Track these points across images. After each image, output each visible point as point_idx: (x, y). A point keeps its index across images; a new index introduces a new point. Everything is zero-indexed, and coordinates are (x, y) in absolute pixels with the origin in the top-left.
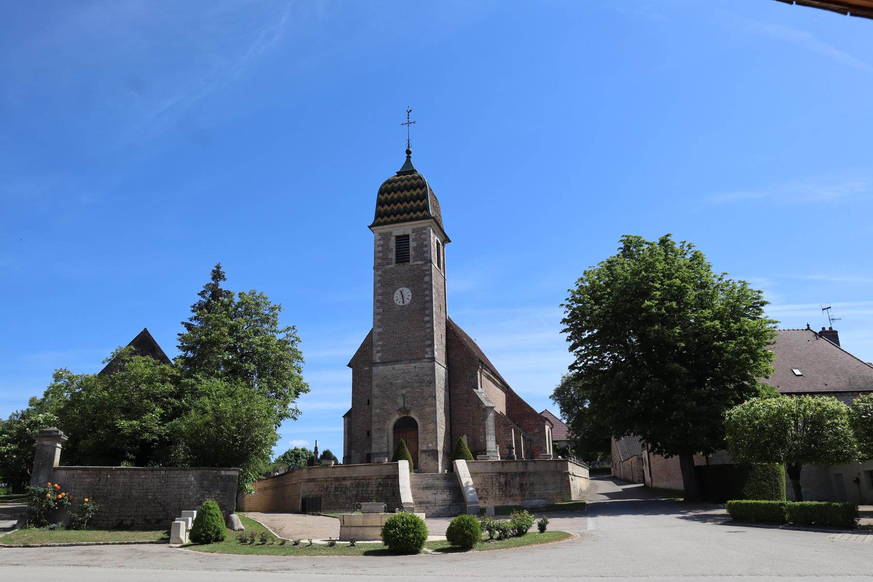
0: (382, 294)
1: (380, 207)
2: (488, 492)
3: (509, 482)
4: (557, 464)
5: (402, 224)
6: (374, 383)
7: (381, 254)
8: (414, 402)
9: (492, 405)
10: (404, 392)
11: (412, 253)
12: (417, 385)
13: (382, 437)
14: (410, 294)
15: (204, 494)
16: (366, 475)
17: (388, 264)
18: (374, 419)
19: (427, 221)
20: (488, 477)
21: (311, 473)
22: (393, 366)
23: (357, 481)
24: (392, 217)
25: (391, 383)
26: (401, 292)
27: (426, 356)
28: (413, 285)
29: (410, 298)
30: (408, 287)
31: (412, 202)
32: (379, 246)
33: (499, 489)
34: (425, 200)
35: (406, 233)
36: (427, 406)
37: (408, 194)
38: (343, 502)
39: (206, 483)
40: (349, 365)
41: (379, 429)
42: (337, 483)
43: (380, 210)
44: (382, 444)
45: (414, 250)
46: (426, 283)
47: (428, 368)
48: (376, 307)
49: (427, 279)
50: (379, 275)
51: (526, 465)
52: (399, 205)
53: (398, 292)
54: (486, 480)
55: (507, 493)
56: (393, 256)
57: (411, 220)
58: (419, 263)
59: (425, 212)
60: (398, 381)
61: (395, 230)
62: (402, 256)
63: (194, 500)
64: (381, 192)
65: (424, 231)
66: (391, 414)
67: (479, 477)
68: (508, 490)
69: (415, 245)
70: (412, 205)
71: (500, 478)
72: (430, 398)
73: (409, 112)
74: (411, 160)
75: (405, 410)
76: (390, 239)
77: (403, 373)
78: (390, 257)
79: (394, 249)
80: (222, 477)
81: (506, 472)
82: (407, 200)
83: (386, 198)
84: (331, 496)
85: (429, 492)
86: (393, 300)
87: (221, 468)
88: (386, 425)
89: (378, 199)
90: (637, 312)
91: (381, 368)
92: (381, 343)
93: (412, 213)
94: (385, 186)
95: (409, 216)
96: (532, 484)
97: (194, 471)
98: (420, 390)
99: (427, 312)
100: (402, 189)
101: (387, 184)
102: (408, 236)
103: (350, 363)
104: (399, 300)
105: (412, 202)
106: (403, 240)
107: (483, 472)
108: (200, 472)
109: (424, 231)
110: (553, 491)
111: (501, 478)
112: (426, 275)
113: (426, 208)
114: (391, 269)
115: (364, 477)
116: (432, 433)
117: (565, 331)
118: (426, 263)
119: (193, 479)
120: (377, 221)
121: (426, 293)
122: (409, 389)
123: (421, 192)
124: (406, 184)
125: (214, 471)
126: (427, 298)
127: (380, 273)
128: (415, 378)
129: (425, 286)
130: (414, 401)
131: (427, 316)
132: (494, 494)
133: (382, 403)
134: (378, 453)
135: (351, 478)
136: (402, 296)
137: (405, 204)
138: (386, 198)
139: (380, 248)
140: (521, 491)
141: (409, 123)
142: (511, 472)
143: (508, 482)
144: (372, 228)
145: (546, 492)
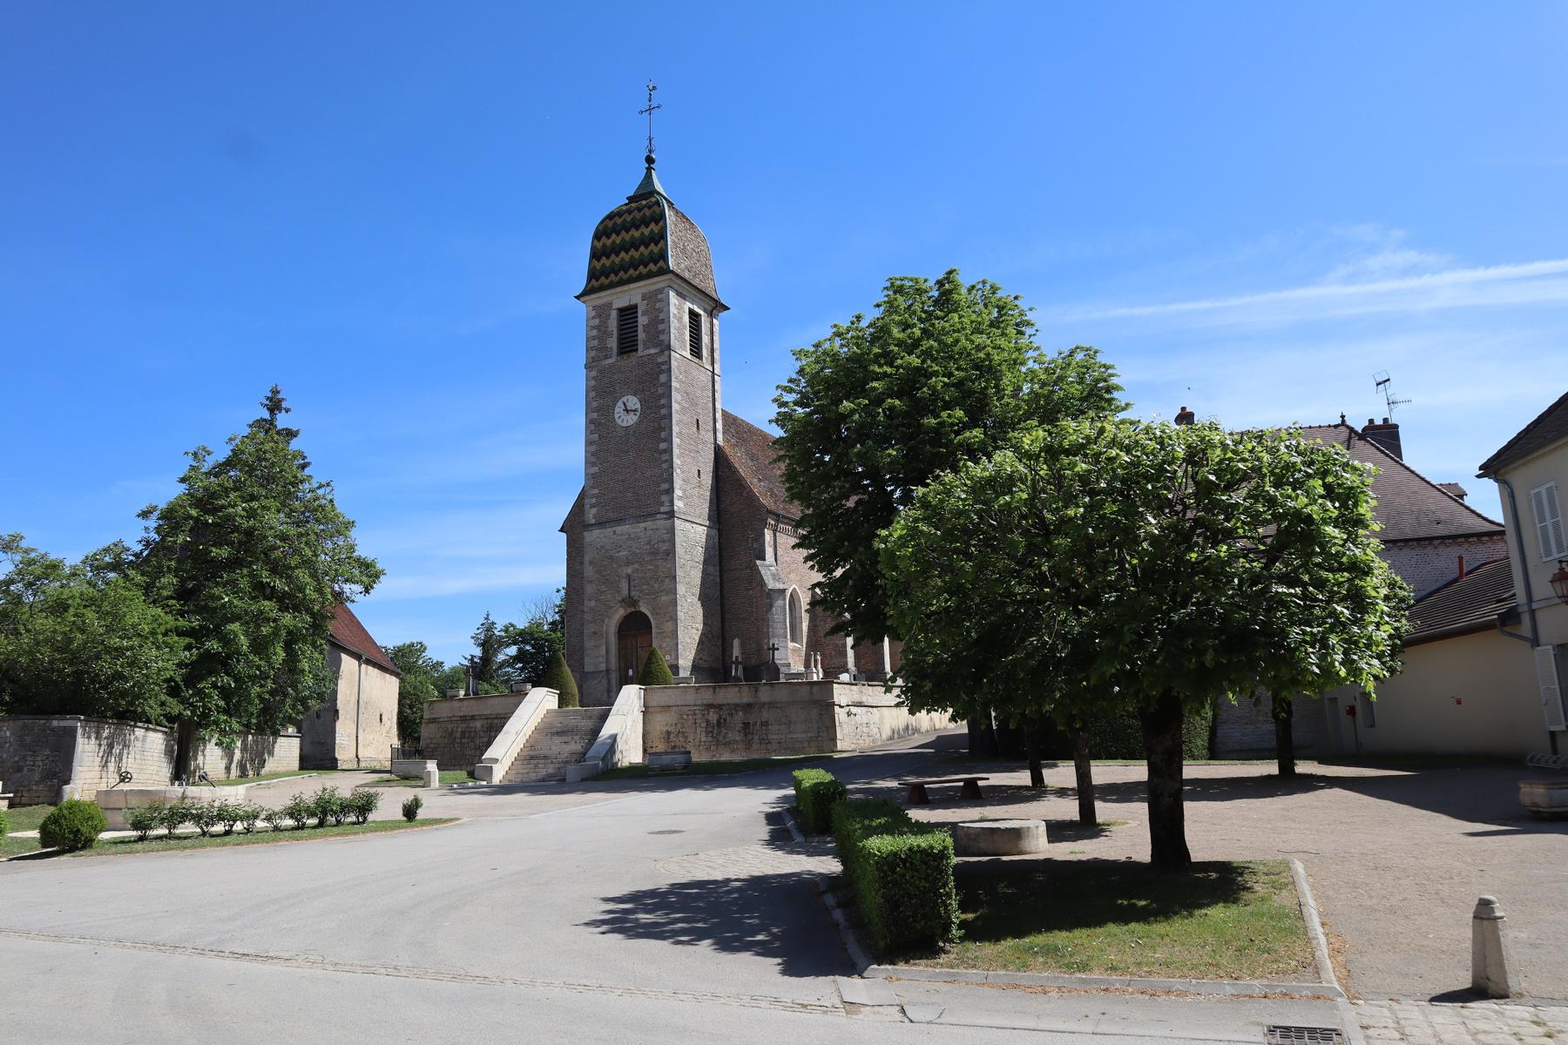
0: (597, 410)
1: (595, 262)
2: (687, 737)
3: (725, 720)
4: (811, 688)
5: (625, 288)
6: (587, 558)
8: (645, 587)
9: (781, 586)
10: (629, 571)
11: (641, 335)
12: (648, 558)
13: (597, 647)
15: (24, 756)
16: (500, 712)
17: (606, 357)
18: (588, 617)
19: (662, 278)
20: (690, 713)
21: (433, 709)
22: (614, 529)
23: (489, 721)
24: (612, 277)
25: (611, 558)
26: (624, 404)
27: (662, 509)
32: (593, 328)
33: (707, 733)
34: (662, 241)
36: (664, 593)
37: (636, 234)
38: (471, 755)
39: (28, 739)
40: (561, 530)
41: (595, 633)
42: (465, 725)
44: (597, 657)
47: (665, 529)
48: (588, 432)
49: (663, 378)
50: (594, 378)
51: (756, 691)
52: (623, 254)
54: (685, 717)
55: (721, 739)
56: (613, 343)
57: (640, 278)
58: (653, 351)
60: (621, 554)
62: (627, 344)
63: (9, 765)
64: (597, 236)
65: (660, 296)
66: (611, 607)
67: (673, 713)
68: (723, 734)
70: (642, 254)
71: (708, 714)
72: (667, 580)
75: (631, 601)
77: (627, 539)
78: (609, 346)
79: (615, 332)
80: (53, 730)
81: (721, 703)
82: (635, 245)
83: (604, 245)
84: (456, 745)
85: (557, 740)
87: (52, 717)
88: (605, 627)
89: (593, 248)
91: (596, 532)
92: (596, 491)
94: (602, 225)
95: (638, 272)
96: (765, 724)
97: (10, 722)
98: (652, 567)
99: (663, 435)
100: (628, 226)
102: (635, 307)
103: (562, 527)
105: (642, 248)
106: (628, 314)
107: (678, 703)
108: (20, 723)
109: (660, 296)
110: (804, 735)
111: (711, 713)
112: (662, 372)
113: (663, 256)
114: (612, 366)
115: (497, 714)
116: (669, 637)
117: (779, 459)
118: (662, 352)
119: (8, 734)
120: (590, 286)
122: (636, 566)
125: (42, 722)
126: (663, 411)
127: (594, 373)
128: (645, 547)
129: (660, 391)
130: (644, 584)
132: (698, 740)
133: (599, 590)
134: (594, 672)
135: (482, 717)
137: (632, 252)
138: (604, 245)
139: (595, 332)
140: (746, 736)
142: (728, 704)
143: (722, 720)
144: (582, 299)
145: (790, 736)
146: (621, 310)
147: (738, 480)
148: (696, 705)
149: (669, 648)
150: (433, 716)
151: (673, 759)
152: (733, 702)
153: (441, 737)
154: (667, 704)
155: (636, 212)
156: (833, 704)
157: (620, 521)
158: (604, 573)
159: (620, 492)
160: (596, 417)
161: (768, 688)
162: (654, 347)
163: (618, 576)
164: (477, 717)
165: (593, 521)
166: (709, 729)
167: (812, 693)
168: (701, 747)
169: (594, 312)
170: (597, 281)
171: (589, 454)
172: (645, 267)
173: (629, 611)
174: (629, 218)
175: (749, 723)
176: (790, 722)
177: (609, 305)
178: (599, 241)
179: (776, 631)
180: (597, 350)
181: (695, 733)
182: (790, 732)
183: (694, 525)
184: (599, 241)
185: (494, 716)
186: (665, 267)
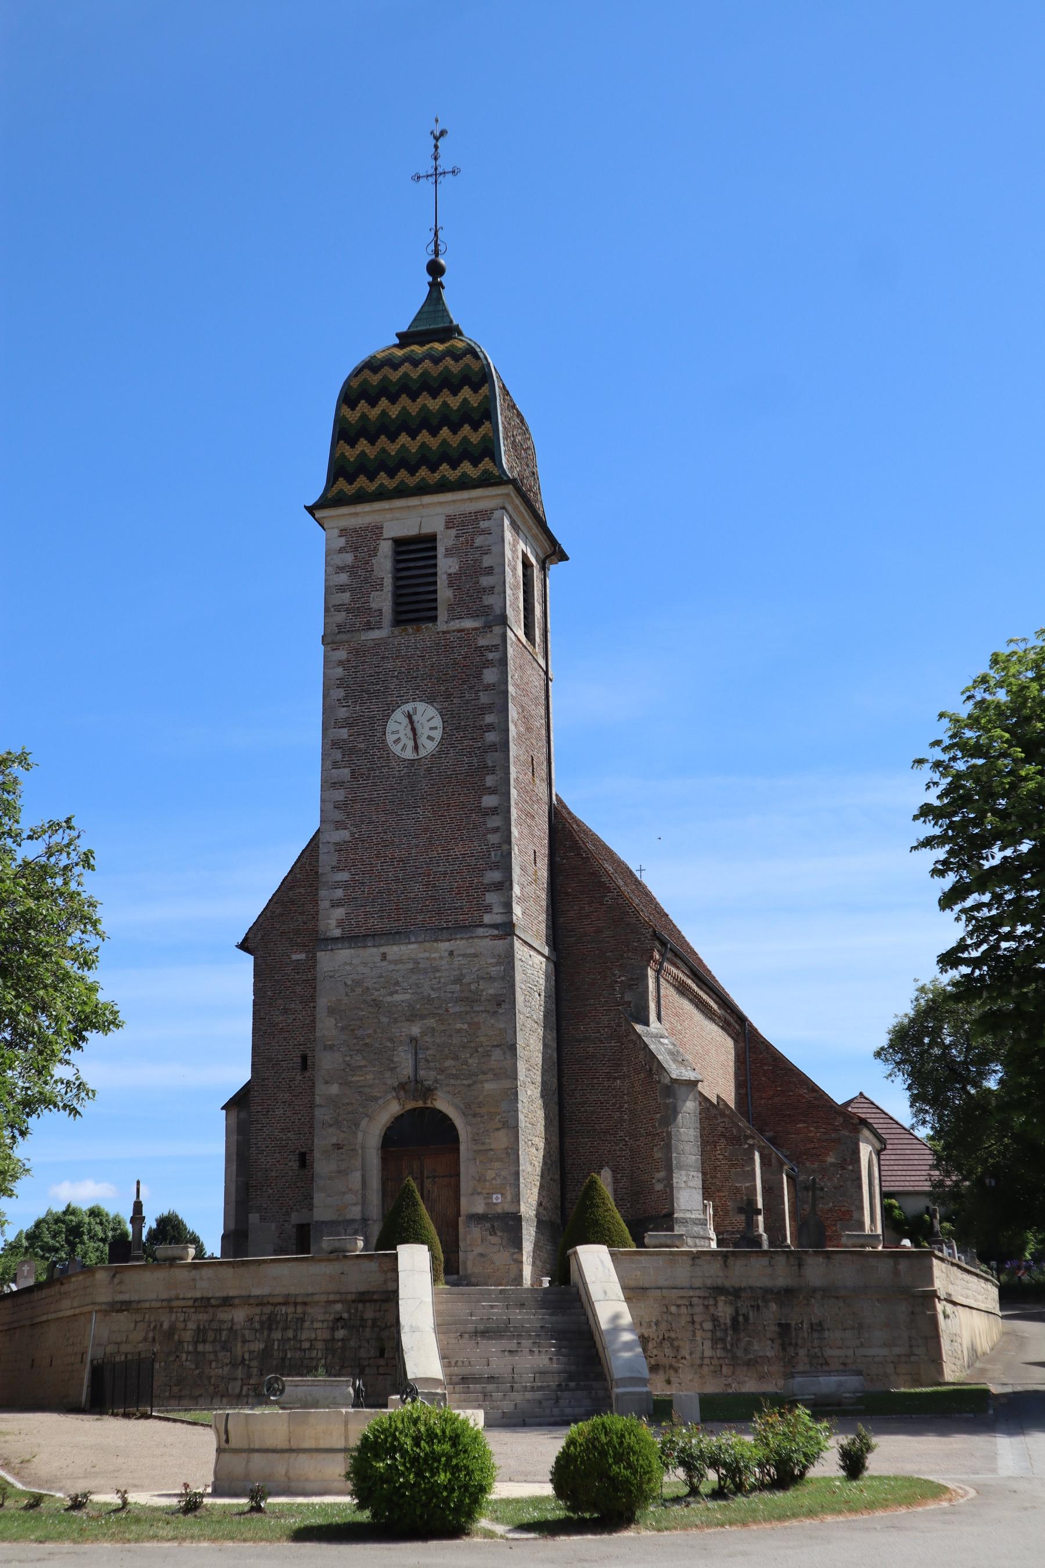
0: (348, 723)
2: (678, 1349)
3: (746, 1318)
5: (414, 501)
6: (323, 1002)
7: (348, 594)
8: (449, 1063)
9: (690, 1075)
10: (415, 1030)
11: (444, 593)
12: (457, 1009)
13: (343, 1173)
14: (438, 722)
17: (369, 627)
18: (322, 1114)
21: (121, 1282)
22: (383, 949)
23: (268, 1310)
25: (377, 1004)
26: (410, 717)
27: (487, 919)
28: (448, 696)
29: (438, 734)
30: (430, 700)
31: (445, 432)
32: (340, 569)
33: (715, 1341)
35: (426, 530)
36: (490, 1076)
37: (433, 405)
41: (338, 1146)
43: (343, 454)
44: (344, 1193)
45: (451, 585)
46: (488, 688)
49: (490, 676)
50: (341, 663)
54: (673, 1309)
55: (740, 1353)
56: (383, 601)
57: (444, 487)
58: (469, 624)
59: (486, 464)
60: (398, 997)
64: (348, 397)
65: (484, 525)
66: (376, 1099)
68: (743, 1344)
69: (455, 569)
71: (716, 1305)
73: (437, 139)
77: (412, 971)
81: (737, 1285)
88: (360, 1135)
89: (340, 422)
91: (344, 954)
92: (344, 876)
93: (445, 466)
94: (360, 378)
95: (437, 476)
96: (818, 1327)
98: (466, 1026)
99: (490, 781)
102: (432, 538)
104: (404, 740)
105: (445, 432)
107: (662, 1283)
109: (484, 525)
110: (884, 1352)
112: (488, 664)
114: (378, 644)
117: (928, 842)
118: (488, 627)
120: (335, 490)
121: (489, 719)
122: (431, 1022)
123: (474, 400)
124: (425, 373)
126: (491, 737)
127: (342, 654)
128: (451, 987)
129: (484, 698)
131: (493, 791)
132: (698, 1355)
135: (247, 1300)
136: (413, 730)
138: (364, 417)
141: (436, 174)
142: (751, 1288)
143: (741, 1319)
144: (319, 514)
146: (400, 544)
147: (593, 873)
148: (691, 1288)
149: (499, 1181)
150: (120, 1298)
151: (840, 1384)
152: (758, 1284)
153: (145, 1339)
154: (641, 1284)
155: (406, 367)
156: (934, 1295)
157: (396, 935)
158: (359, 1033)
159: (397, 880)
160: (346, 736)
161: (821, 1259)
162: (474, 616)
163: (391, 1040)
164: (237, 1301)
165: (337, 933)
166: (719, 1334)
167: (896, 1273)
168: (706, 1369)
169: (343, 540)
170: (351, 483)
171: (330, 806)
172: (454, 466)
173: (411, 1105)
174: (395, 376)
175: (788, 1325)
176: (861, 1326)
177: (376, 531)
178: (353, 408)
179: (683, 1158)
180: (348, 611)
181: (693, 1340)
182: (862, 1345)
183: (532, 953)
184: (353, 408)
185: (280, 1300)
186: (496, 472)
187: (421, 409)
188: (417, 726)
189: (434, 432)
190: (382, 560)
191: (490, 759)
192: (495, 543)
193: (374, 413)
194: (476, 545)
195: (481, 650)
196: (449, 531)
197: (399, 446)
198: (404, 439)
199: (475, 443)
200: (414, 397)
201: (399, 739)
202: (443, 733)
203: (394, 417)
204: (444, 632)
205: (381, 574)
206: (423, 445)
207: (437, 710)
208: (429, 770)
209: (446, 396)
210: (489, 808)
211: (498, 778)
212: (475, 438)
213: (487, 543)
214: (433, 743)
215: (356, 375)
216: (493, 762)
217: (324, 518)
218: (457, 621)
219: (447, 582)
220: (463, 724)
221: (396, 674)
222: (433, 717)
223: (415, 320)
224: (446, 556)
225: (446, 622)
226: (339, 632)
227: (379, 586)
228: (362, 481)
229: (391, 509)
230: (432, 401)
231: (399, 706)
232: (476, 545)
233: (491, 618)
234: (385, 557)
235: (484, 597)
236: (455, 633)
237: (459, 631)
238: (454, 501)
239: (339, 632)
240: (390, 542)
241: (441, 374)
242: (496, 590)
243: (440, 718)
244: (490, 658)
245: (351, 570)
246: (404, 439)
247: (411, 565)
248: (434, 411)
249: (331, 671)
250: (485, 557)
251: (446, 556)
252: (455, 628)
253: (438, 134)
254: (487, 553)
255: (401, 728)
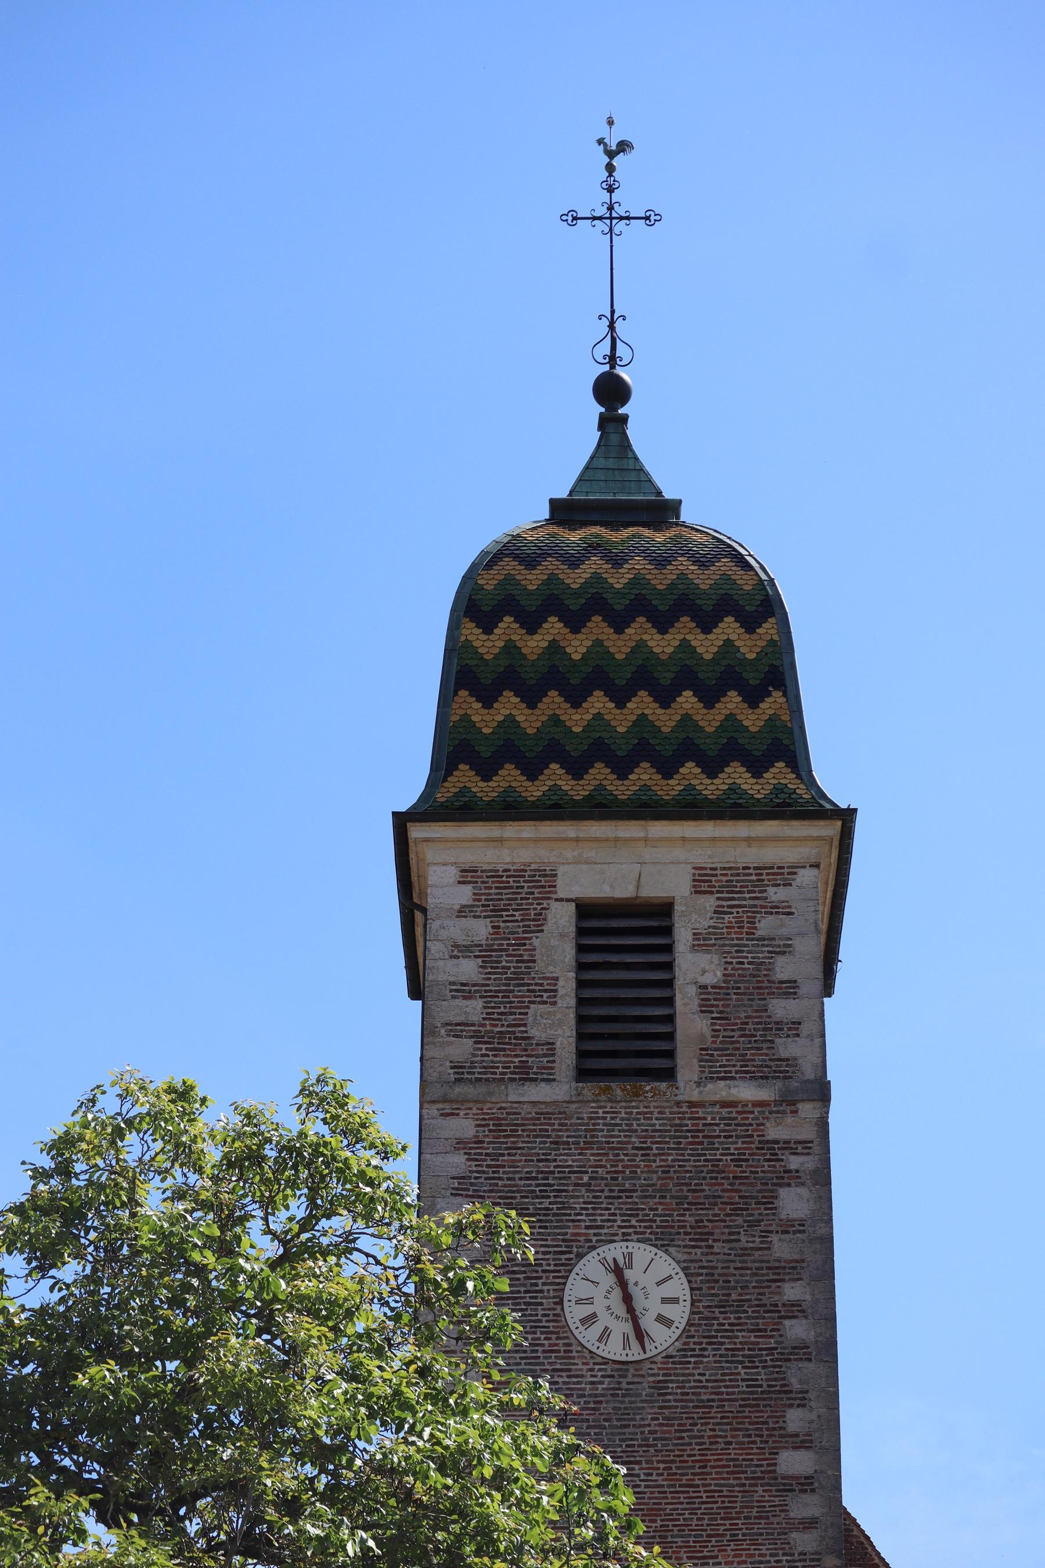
1: (468, 704)
7: (478, 1004)
14: (679, 1287)
17: (525, 1076)
26: (618, 1272)
28: (702, 1237)
29: (679, 1314)
30: (663, 1241)
31: (687, 700)
35: (653, 891)
43: (466, 718)
45: (705, 1008)
46: (788, 1227)
50: (460, 1144)
53: (591, 1266)
58: (746, 1092)
59: (778, 774)
61: (577, 862)
65: (775, 894)
69: (713, 976)
73: (611, 154)
74: (632, 431)
76: (540, 918)
86: (559, 1317)
90: (214, 1274)
93: (690, 769)
99: (795, 1420)
101: (510, 566)
104: (604, 1320)
105: (687, 700)
109: (775, 894)
112: (789, 1178)
114: (545, 1113)
118: (788, 1102)
121: (792, 1291)
123: (749, 647)
124: (637, 581)
126: (797, 1330)
127: (465, 1127)
129: (781, 1248)
131: (802, 1443)
136: (627, 1299)
141: (611, 217)
155: (594, 565)
162: (759, 1077)
169: (467, 891)
172: (712, 770)
180: (478, 1038)
187: (634, 650)
188: (635, 1291)
189: (665, 698)
190: (554, 942)
191: (795, 1376)
192: (801, 934)
193: (534, 645)
194: (759, 933)
195: (774, 1149)
196: (702, 899)
197: (589, 717)
198: (598, 703)
199: (753, 729)
200: (619, 625)
201: (594, 1315)
202: (692, 1313)
203: (576, 657)
204: (692, 1104)
205: (552, 971)
206: (642, 720)
207: (678, 1262)
208: (659, 1387)
209: (685, 630)
210: (793, 1478)
211: (813, 1416)
212: (752, 720)
213: (784, 931)
214: (669, 1332)
215: (489, 566)
216: (801, 1382)
217: (427, 840)
218: (722, 1083)
219: (696, 1002)
220: (734, 1297)
221: (586, 1179)
222: (670, 1277)
223: (580, 480)
224: (694, 948)
225: (698, 1084)
226: (457, 1080)
227: (548, 993)
228: (509, 776)
229: (577, 840)
230: (658, 637)
231: (594, 1248)
232: (759, 933)
233: (794, 1084)
234: (562, 936)
235: (778, 1040)
236: (716, 1109)
237: (725, 1104)
238: (714, 839)
239: (457, 1080)
240: (574, 904)
241: (672, 586)
242: (804, 1029)
243: (684, 1280)
244: (793, 1166)
245: (486, 954)
246: (598, 703)
247: (614, 958)
248: (663, 657)
249: (440, 1158)
250: (780, 960)
251: (694, 948)
252: (717, 1098)
253: (614, 148)
254: (784, 953)
255: (598, 1293)
